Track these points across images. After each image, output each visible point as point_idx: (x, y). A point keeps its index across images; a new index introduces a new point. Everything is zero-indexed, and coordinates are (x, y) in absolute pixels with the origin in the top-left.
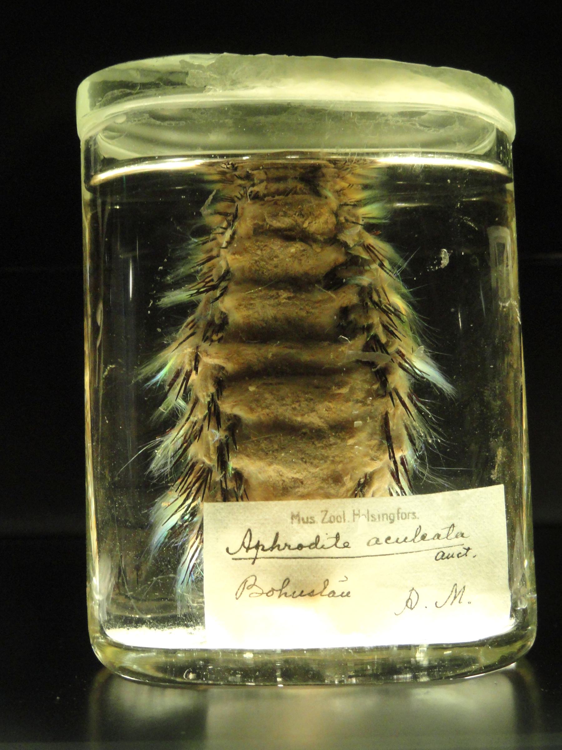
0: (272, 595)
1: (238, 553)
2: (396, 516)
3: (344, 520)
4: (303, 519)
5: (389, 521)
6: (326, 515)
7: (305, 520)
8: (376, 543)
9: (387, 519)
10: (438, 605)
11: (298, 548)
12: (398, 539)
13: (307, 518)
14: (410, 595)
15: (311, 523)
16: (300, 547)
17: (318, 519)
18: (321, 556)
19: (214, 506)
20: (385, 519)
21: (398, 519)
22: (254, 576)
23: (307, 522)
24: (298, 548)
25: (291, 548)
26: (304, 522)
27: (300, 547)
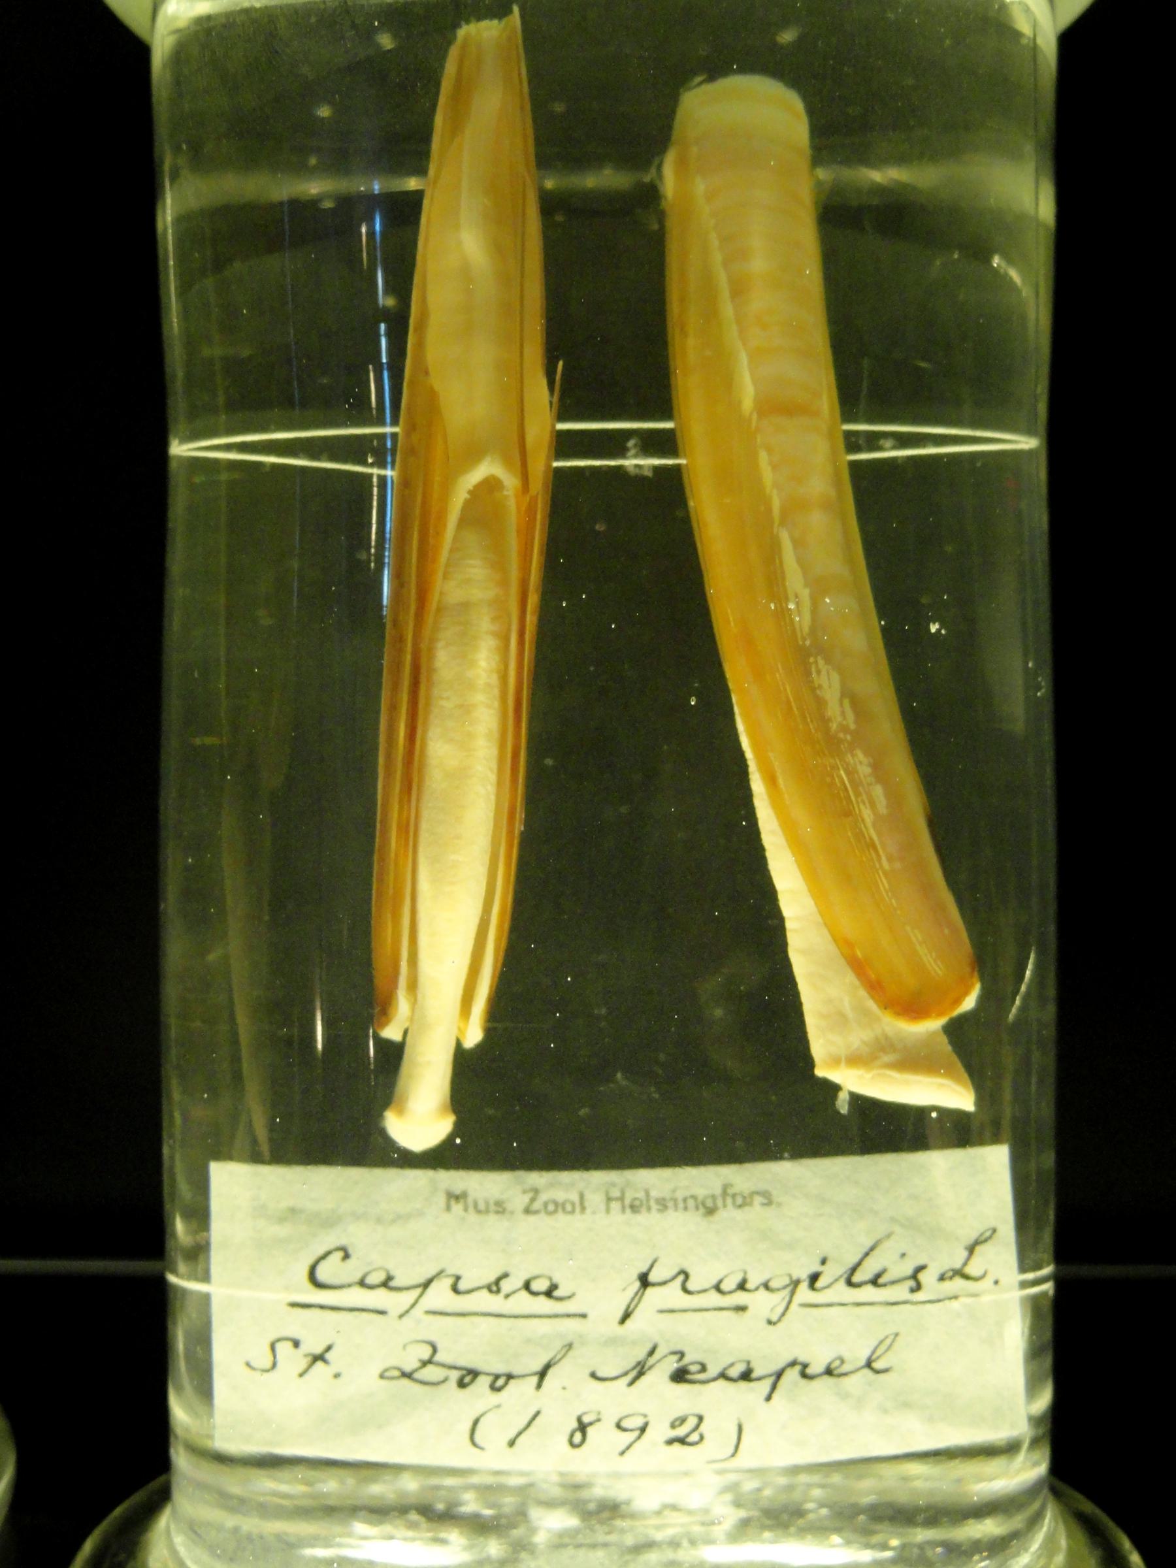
3: (583, 1209)
23: (487, 1211)
26: (479, 1212)
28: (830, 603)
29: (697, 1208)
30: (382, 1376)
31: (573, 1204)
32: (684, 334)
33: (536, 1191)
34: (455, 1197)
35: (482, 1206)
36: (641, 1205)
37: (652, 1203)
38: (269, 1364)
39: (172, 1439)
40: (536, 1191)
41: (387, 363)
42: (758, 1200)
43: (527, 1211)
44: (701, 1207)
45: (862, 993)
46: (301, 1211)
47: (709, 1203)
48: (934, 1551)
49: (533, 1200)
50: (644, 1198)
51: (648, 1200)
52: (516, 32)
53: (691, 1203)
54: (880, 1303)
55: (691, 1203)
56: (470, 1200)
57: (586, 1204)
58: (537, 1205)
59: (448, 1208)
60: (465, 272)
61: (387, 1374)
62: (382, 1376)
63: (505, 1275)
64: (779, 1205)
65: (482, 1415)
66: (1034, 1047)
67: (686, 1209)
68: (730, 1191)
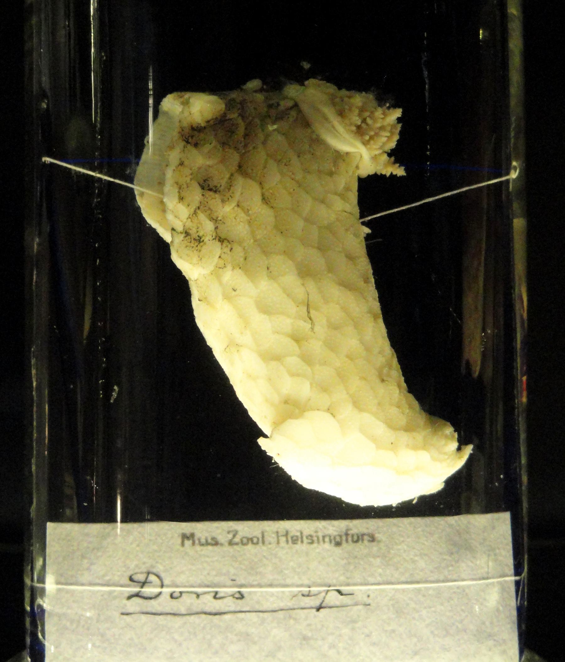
3: (263, 542)
28: (428, 145)
29: (331, 542)
31: (258, 539)
34: (185, 537)
35: (203, 541)
36: (297, 540)
37: (305, 538)
39: (25, 587)
46: (239, 163)
47: (338, 539)
48: (360, 125)
49: (234, 536)
50: (300, 536)
52: (37, 494)
53: (327, 539)
55: (327, 539)
57: (265, 539)
58: (237, 540)
59: (183, 544)
60: (40, 602)
64: (379, 542)
66: (517, 403)
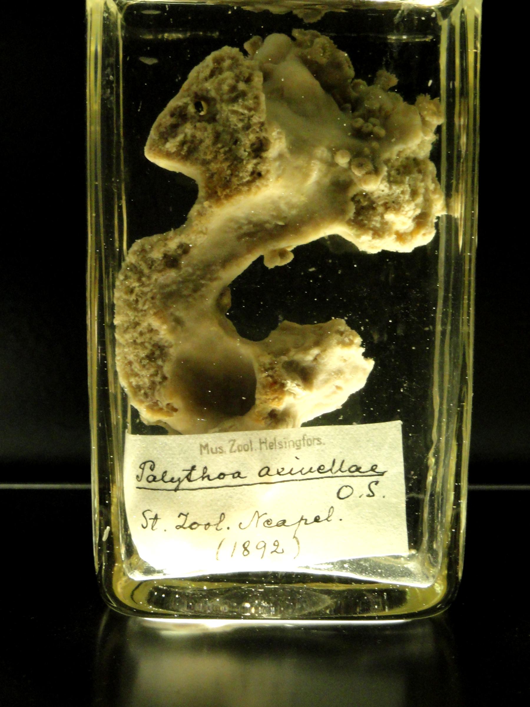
0: (224, 517)
1: (285, 475)
2: (302, 442)
3: (252, 449)
4: (212, 449)
5: (296, 447)
6: (233, 445)
7: (214, 450)
8: (267, 474)
9: (294, 445)
10: (258, 548)
11: (219, 477)
12: (311, 468)
13: (216, 449)
14: (295, 533)
15: (221, 453)
16: (222, 476)
17: (227, 449)
18: (159, 488)
19: (247, 435)
20: (292, 446)
21: (304, 446)
22: (340, 498)
23: (216, 453)
24: (219, 477)
25: (211, 478)
26: (213, 453)
27: (222, 476)
30: (332, 507)
32: (99, 117)
33: (234, 441)
38: (145, 513)
40: (234, 441)
41: (191, 31)
42: (316, 441)
43: (231, 451)
44: (295, 445)
45: (260, 342)
51: (275, 443)
54: (253, 519)
56: (209, 448)
58: (235, 448)
61: (223, 516)
62: (332, 507)
63: (303, 468)
65: (222, 542)
67: (286, 447)
68: (306, 438)
